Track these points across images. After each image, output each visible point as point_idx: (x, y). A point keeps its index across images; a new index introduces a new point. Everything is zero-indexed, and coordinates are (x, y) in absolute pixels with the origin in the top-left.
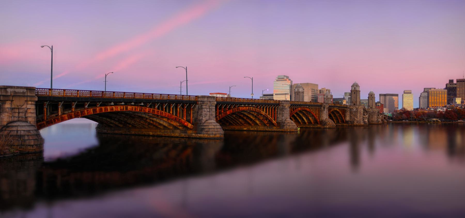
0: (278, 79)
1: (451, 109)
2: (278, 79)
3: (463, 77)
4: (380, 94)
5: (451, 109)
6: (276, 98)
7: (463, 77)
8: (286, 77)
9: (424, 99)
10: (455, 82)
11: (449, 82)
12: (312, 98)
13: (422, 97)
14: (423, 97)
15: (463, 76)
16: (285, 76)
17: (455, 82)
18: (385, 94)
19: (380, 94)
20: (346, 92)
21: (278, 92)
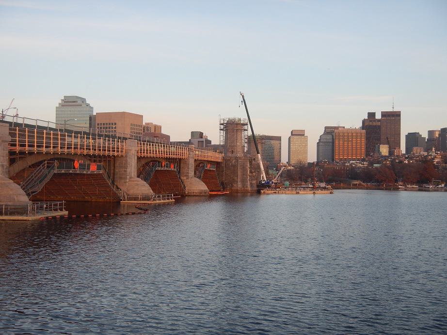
7: (393, 108)
10: (378, 116)
17: (378, 116)
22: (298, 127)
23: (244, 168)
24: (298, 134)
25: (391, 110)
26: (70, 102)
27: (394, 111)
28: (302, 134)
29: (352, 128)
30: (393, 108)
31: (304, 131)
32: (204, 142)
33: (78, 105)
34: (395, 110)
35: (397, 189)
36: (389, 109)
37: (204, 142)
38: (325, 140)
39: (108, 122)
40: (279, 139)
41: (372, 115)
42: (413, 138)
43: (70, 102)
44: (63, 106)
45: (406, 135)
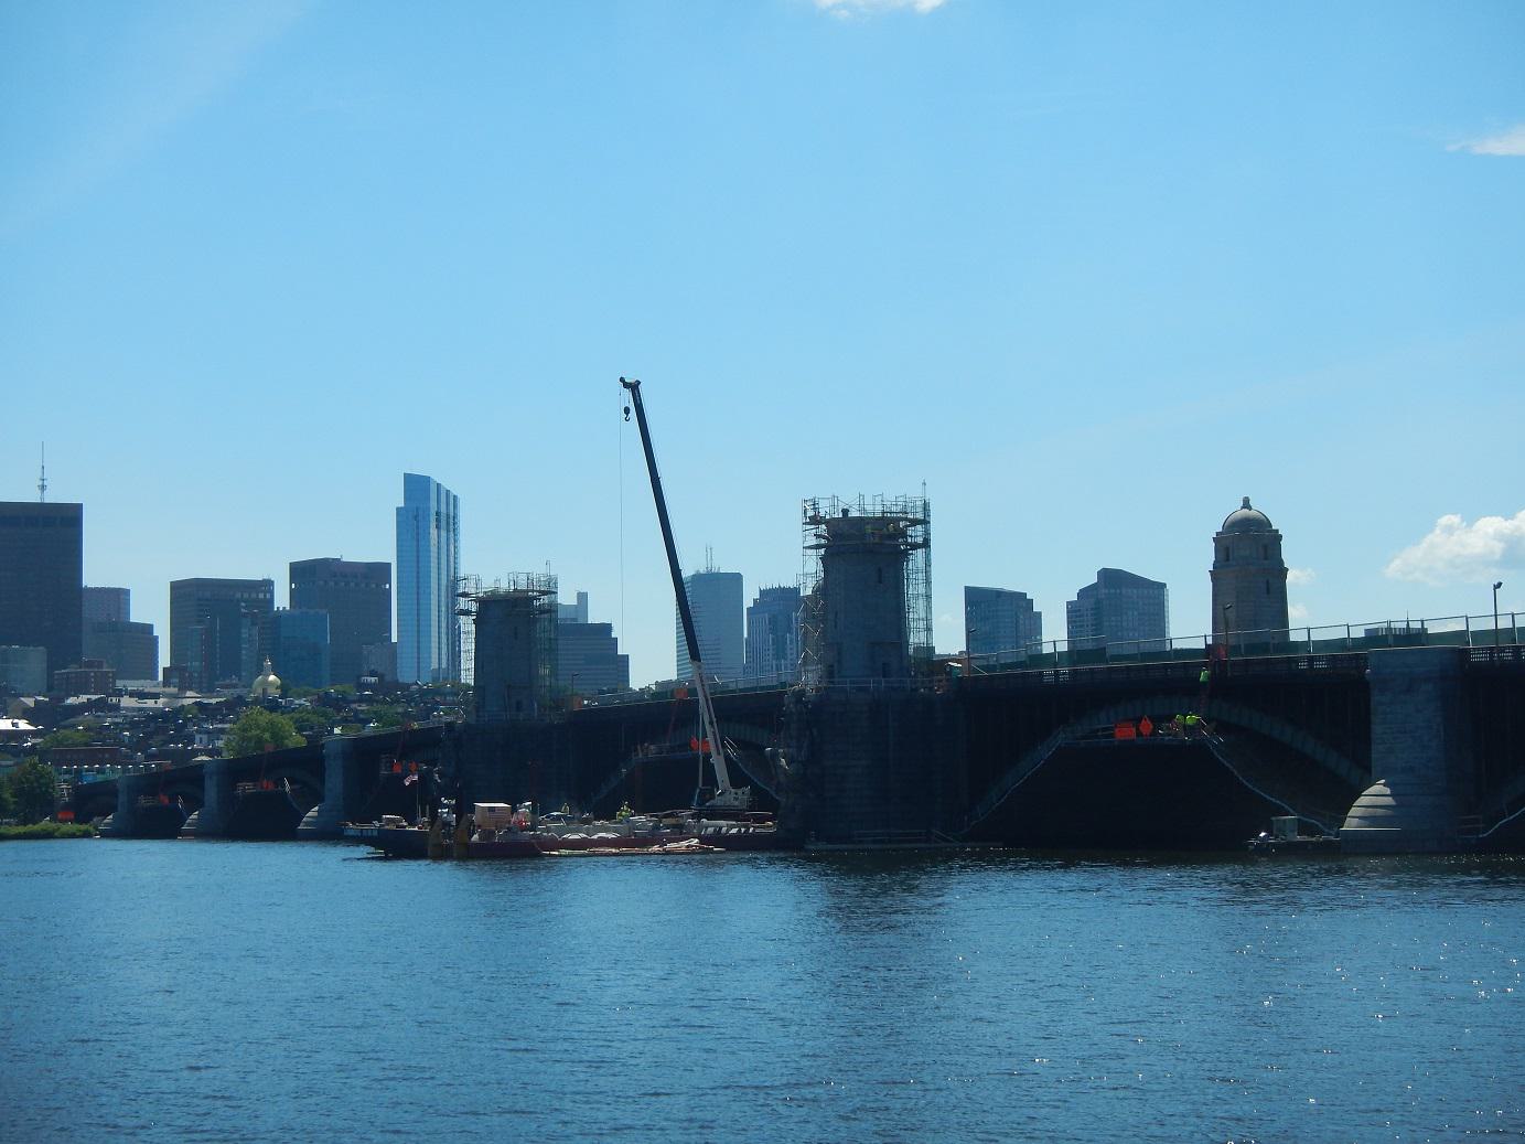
7: (43, 488)
25: (32, 497)
30: (43, 488)
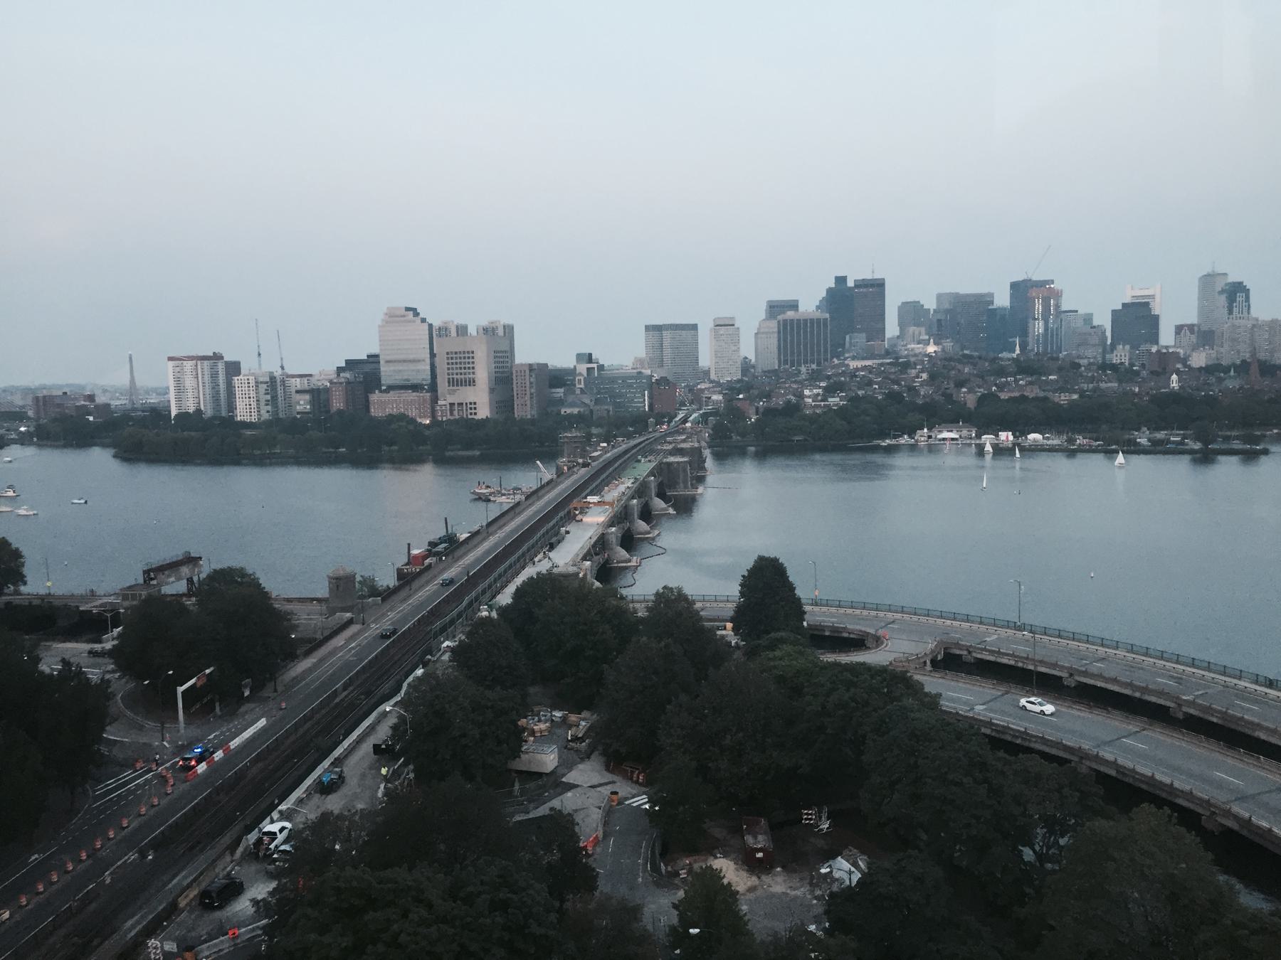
0: (389, 317)
1: (646, 392)
2: (389, 317)
3: (873, 272)
4: (696, 325)
5: (646, 392)
6: (1082, 714)
7: (873, 272)
8: (412, 312)
9: (767, 338)
10: (850, 283)
11: (834, 281)
12: (497, 375)
13: (763, 333)
14: (766, 333)
15: (873, 269)
16: (408, 309)
17: (850, 283)
18: (661, 324)
19: (698, 326)
20: (699, 328)
21: (825, 340)
22: (724, 313)
23: (685, 471)
24: (725, 325)
25: (869, 277)
26: (397, 316)
27: (875, 278)
28: (731, 323)
29: (808, 311)
31: (733, 318)
32: (596, 369)
33: (410, 322)
34: (877, 276)
35: (528, 579)
36: (867, 275)
37: (596, 369)
38: (767, 330)
39: (461, 349)
40: (694, 327)
41: (841, 280)
42: (912, 312)
43: (397, 316)
44: (387, 322)
45: (1242, 283)
